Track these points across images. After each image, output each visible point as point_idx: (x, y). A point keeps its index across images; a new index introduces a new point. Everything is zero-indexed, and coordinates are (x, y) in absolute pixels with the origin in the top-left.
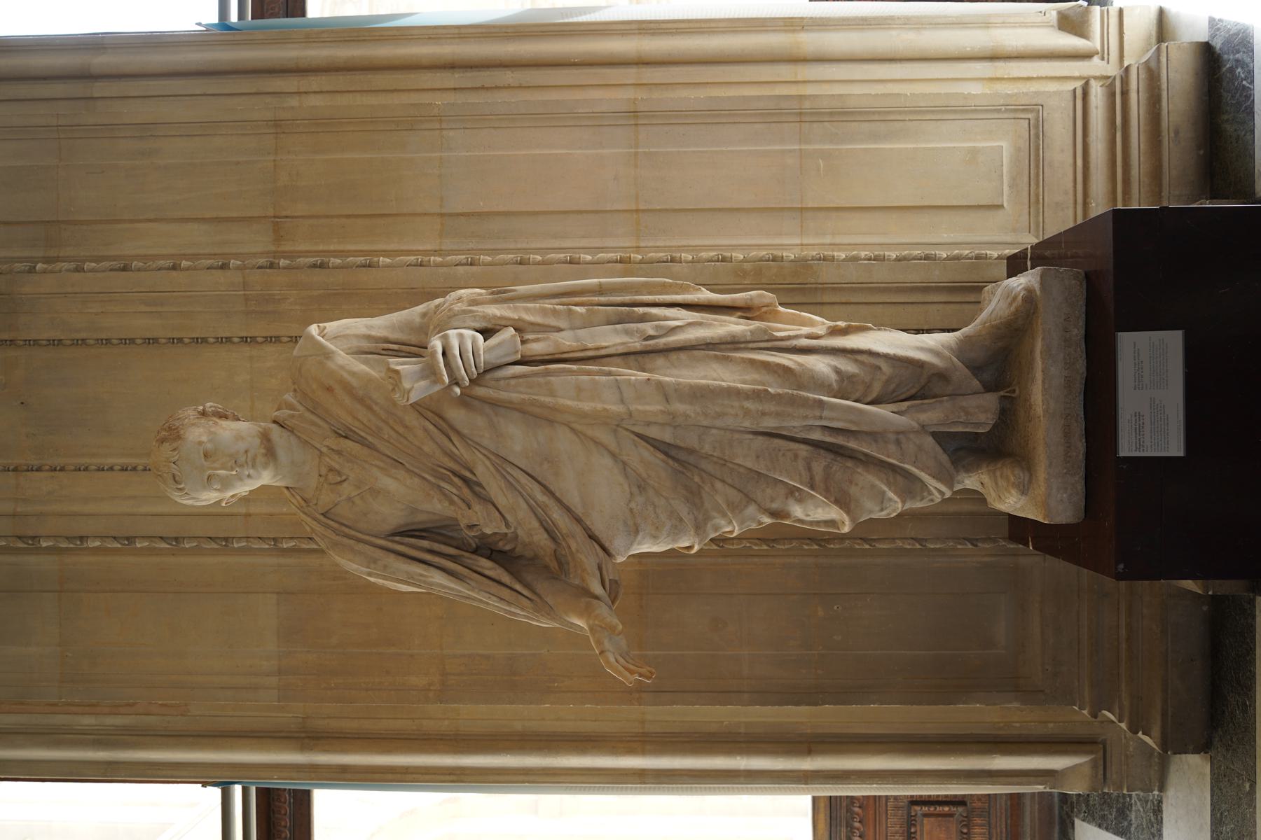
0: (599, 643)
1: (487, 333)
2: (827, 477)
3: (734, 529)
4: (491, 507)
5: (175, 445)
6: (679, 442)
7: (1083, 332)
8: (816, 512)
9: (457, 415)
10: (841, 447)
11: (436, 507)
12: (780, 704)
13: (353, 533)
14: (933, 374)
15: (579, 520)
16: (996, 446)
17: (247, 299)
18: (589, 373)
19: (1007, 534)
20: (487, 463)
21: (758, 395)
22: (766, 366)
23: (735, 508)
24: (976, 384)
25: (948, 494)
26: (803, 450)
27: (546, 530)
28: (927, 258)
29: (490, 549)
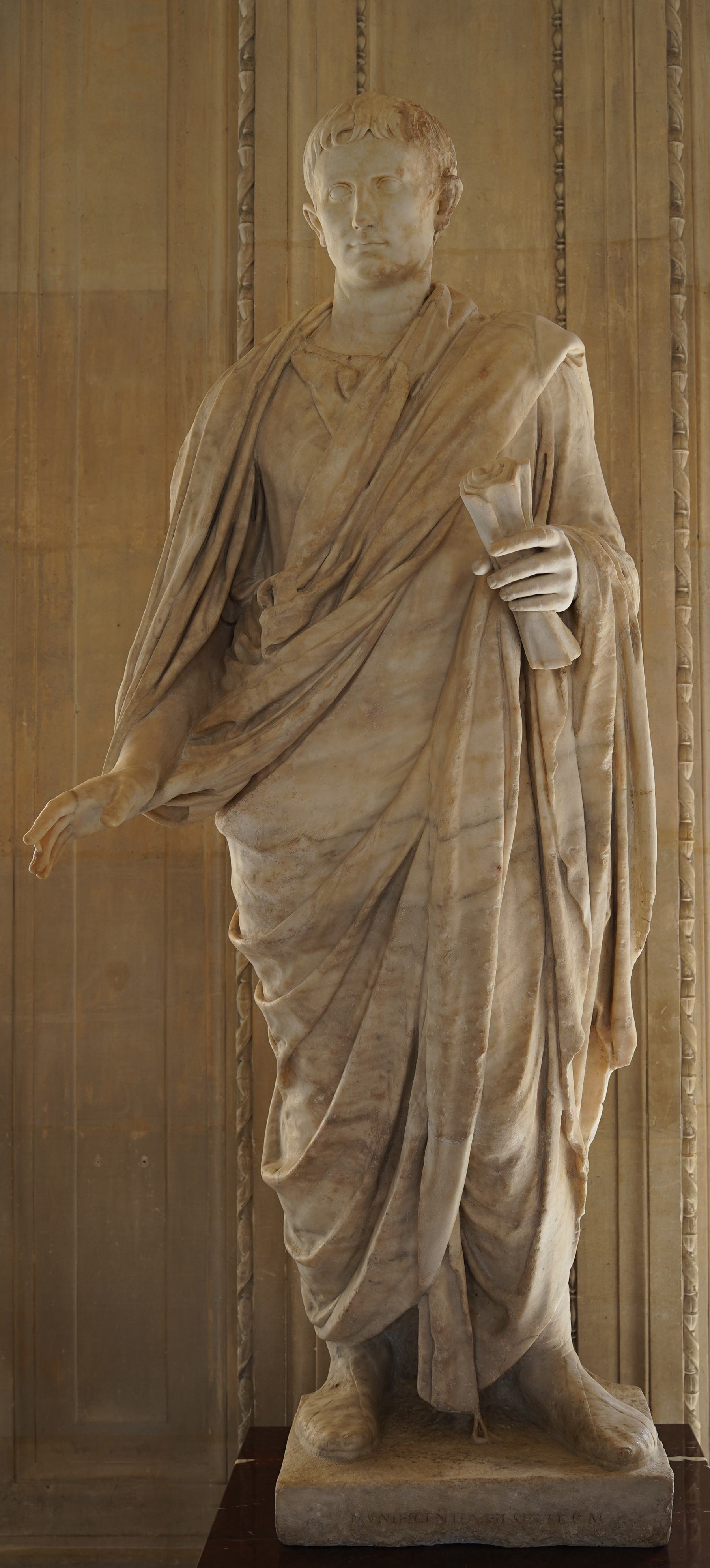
0: (90, 791)
1: (571, 616)
2: (347, 1145)
3: (267, 998)
4: (301, 622)
5: (397, 132)
6: (401, 915)
7: (573, 1543)
8: (293, 1127)
9: (443, 570)
10: (394, 1167)
11: (300, 537)
13: (261, 408)
15: (280, 759)
16: (395, 1407)
17: (625, 243)
18: (509, 775)
19: (257, 1424)
20: (370, 617)
21: (474, 1038)
22: (521, 1050)
23: (299, 1002)
24: (492, 1376)
25: (321, 1333)
26: (389, 1108)
27: (265, 709)
28: (688, 1300)
29: (235, 620)
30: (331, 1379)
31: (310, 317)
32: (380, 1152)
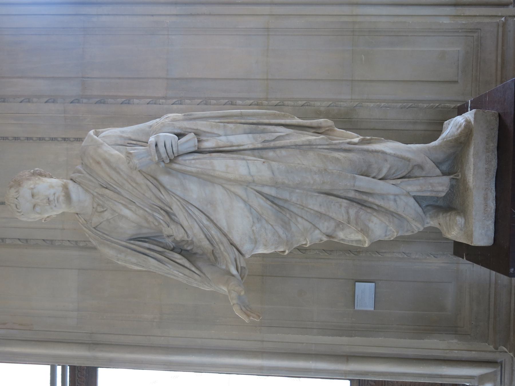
1: (180, 135)
2: (357, 217)
4: (179, 226)
6: (279, 196)
7: (496, 145)
10: (366, 201)
12: (333, 335)
13: (109, 238)
14: (415, 165)
19: (452, 253)
20: (179, 203)
24: (438, 172)
25: (422, 229)
26: (345, 202)
27: (208, 239)
30: (437, 226)
31: (81, 221)
32: (360, 206)
